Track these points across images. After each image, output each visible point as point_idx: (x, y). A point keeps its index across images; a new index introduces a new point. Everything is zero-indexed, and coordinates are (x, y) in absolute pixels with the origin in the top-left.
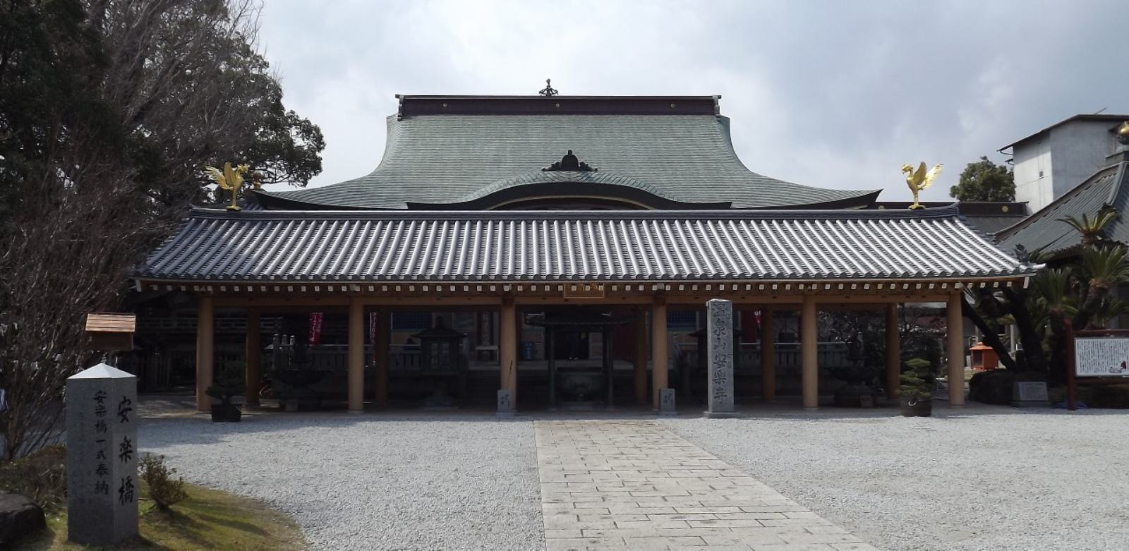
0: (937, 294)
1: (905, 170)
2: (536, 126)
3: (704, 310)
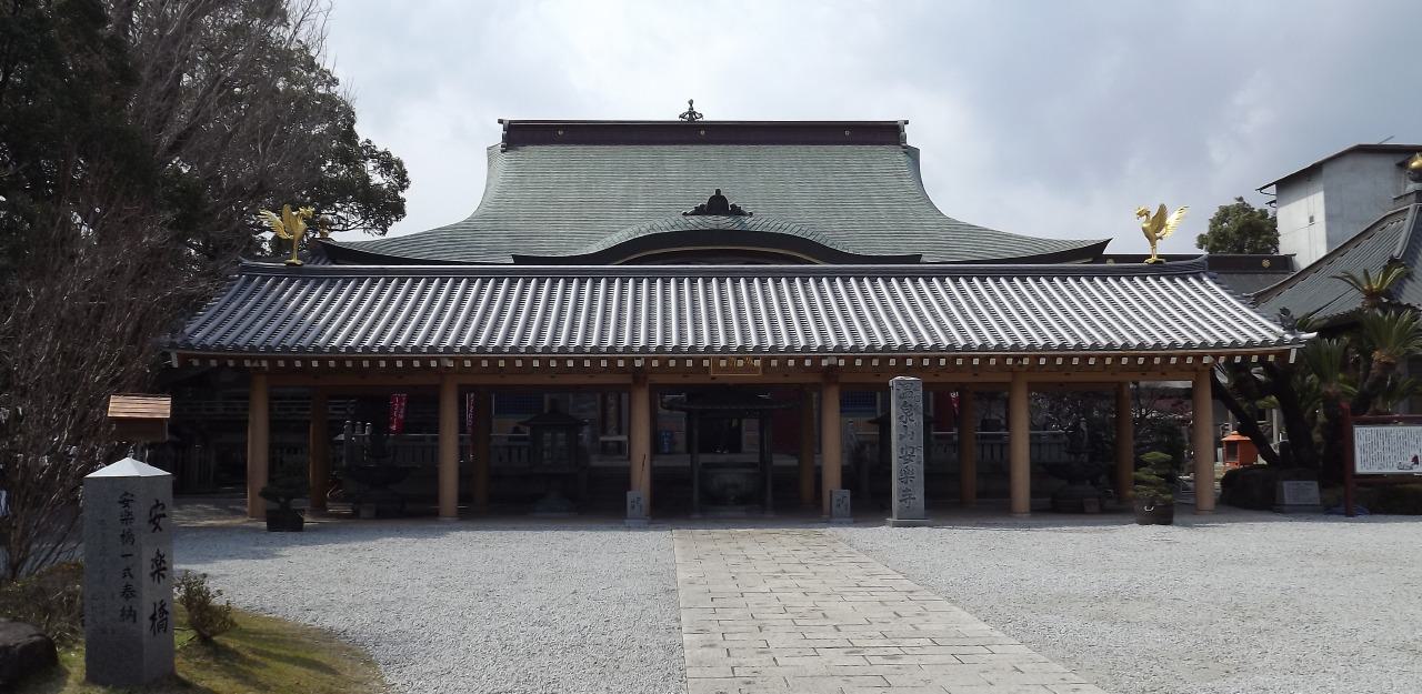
0: (1180, 370)
1: (1140, 214)
2: (676, 160)
3: (887, 390)
